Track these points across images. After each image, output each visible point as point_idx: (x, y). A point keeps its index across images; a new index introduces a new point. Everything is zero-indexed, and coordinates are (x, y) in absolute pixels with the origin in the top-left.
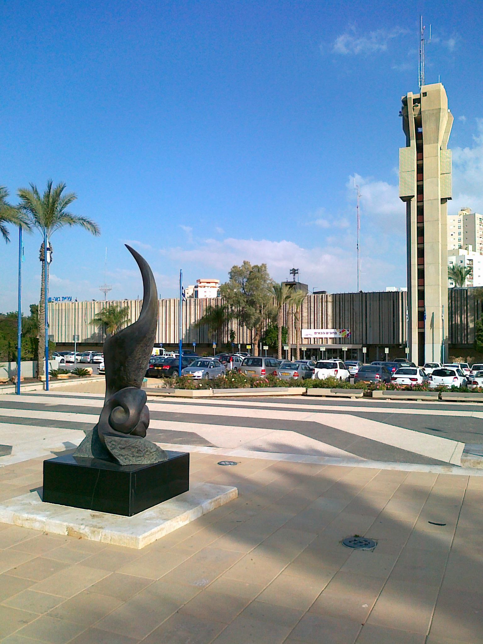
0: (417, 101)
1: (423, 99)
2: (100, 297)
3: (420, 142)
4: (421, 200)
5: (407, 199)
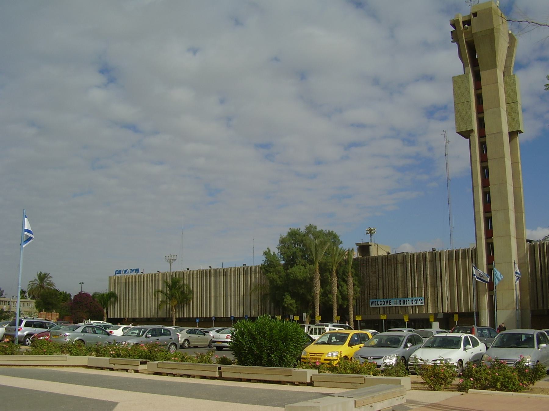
0: (468, 22)
1: (474, 20)
2: (165, 268)
3: (481, 115)
4: (482, 134)
5: (467, 134)
